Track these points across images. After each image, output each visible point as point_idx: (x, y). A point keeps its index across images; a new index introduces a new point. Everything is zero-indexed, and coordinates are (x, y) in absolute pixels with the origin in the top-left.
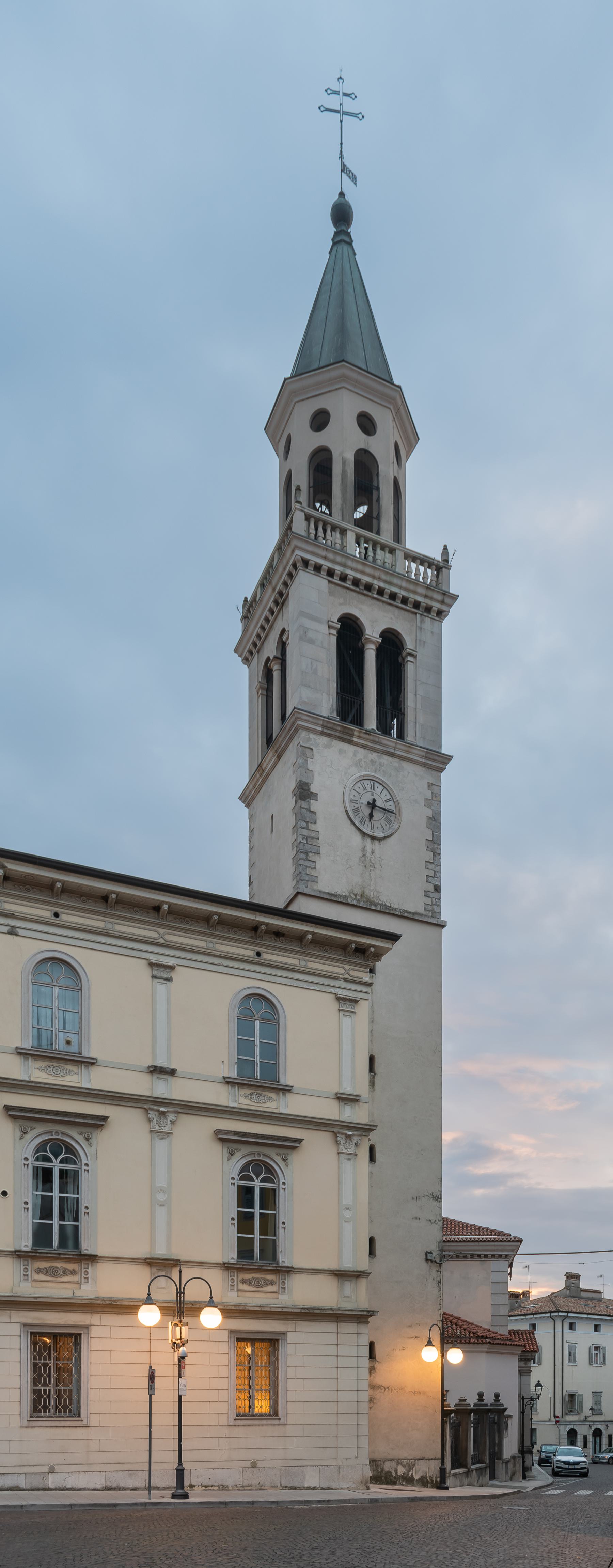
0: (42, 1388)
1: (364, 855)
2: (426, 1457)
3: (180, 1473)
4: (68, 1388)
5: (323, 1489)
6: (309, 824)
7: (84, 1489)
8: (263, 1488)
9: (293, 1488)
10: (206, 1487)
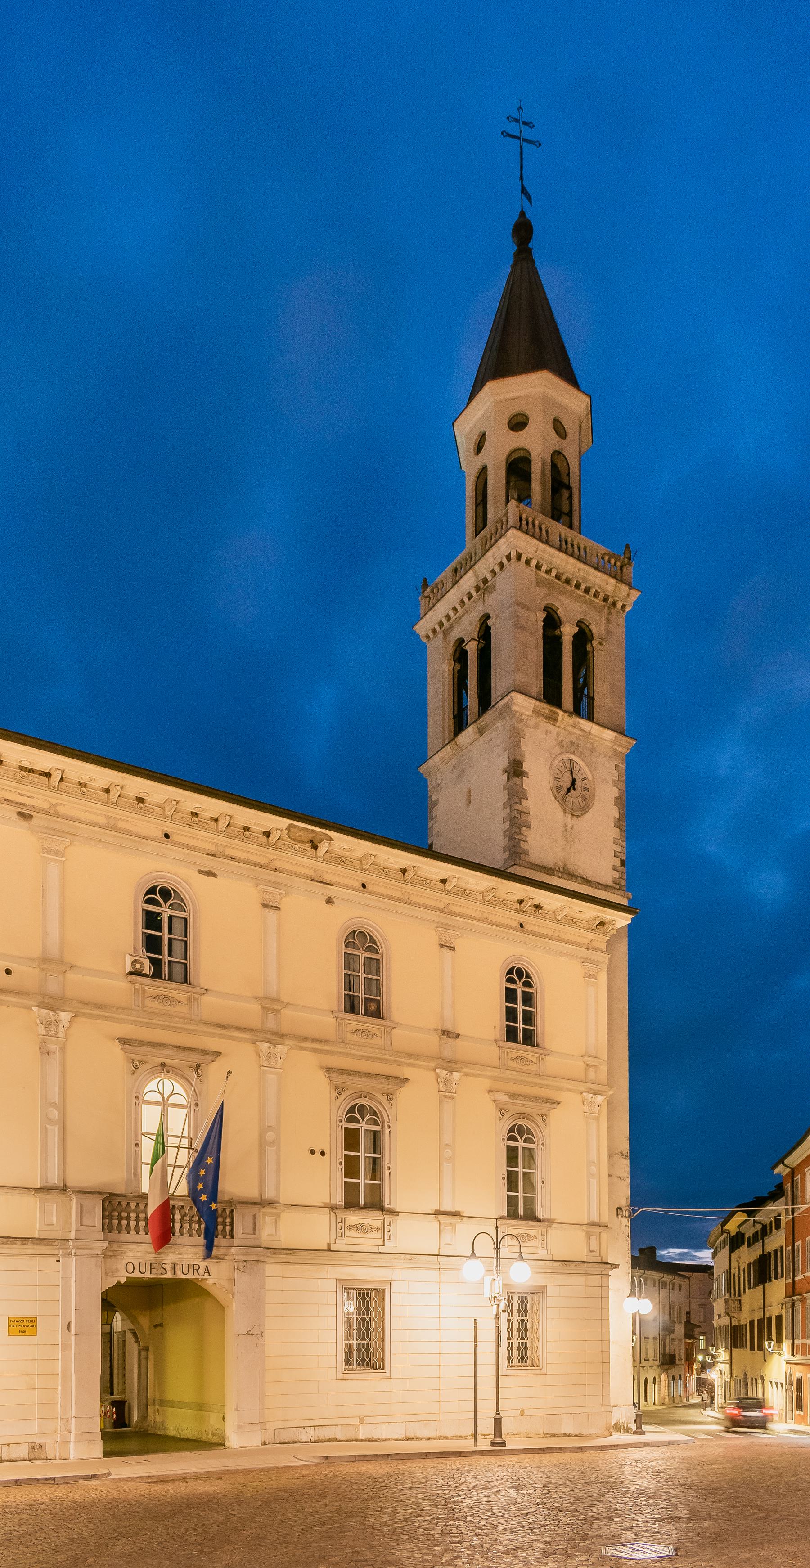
0: (361, 1342)
1: (566, 830)
2: (619, 1404)
3: (498, 1422)
4: (366, 1342)
5: (576, 1436)
6: (522, 799)
7: (388, 1440)
8: (529, 1435)
9: (553, 1436)
10: (484, 1435)
